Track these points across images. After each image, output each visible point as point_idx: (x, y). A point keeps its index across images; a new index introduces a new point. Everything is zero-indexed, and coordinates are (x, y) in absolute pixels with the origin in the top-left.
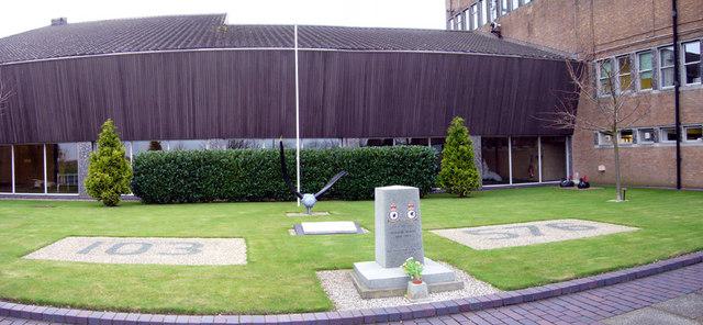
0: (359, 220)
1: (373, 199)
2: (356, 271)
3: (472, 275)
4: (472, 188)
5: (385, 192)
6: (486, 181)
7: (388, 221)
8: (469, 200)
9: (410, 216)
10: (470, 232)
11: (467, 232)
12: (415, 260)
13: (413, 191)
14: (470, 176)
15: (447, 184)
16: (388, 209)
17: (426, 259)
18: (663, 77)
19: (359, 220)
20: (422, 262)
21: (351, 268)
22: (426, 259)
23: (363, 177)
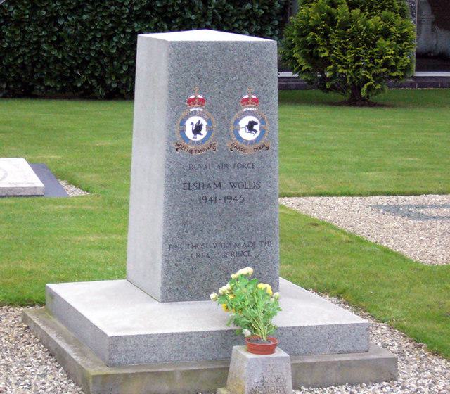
0: (51, 157)
1: (123, 91)
2: (65, 314)
3: (417, 339)
4: (391, 74)
5: (174, 45)
6: (428, 59)
7: (178, 145)
8: (378, 111)
9: (249, 136)
10: (396, 210)
11: (388, 209)
12: (258, 277)
13: (265, 46)
14: (386, 34)
15: (313, 58)
16: (180, 103)
17: (283, 282)
18: (55, 203)
19: (51, 157)
20: (275, 287)
21: (40, 301)
22: (283, 282)
23: (53, 19)
